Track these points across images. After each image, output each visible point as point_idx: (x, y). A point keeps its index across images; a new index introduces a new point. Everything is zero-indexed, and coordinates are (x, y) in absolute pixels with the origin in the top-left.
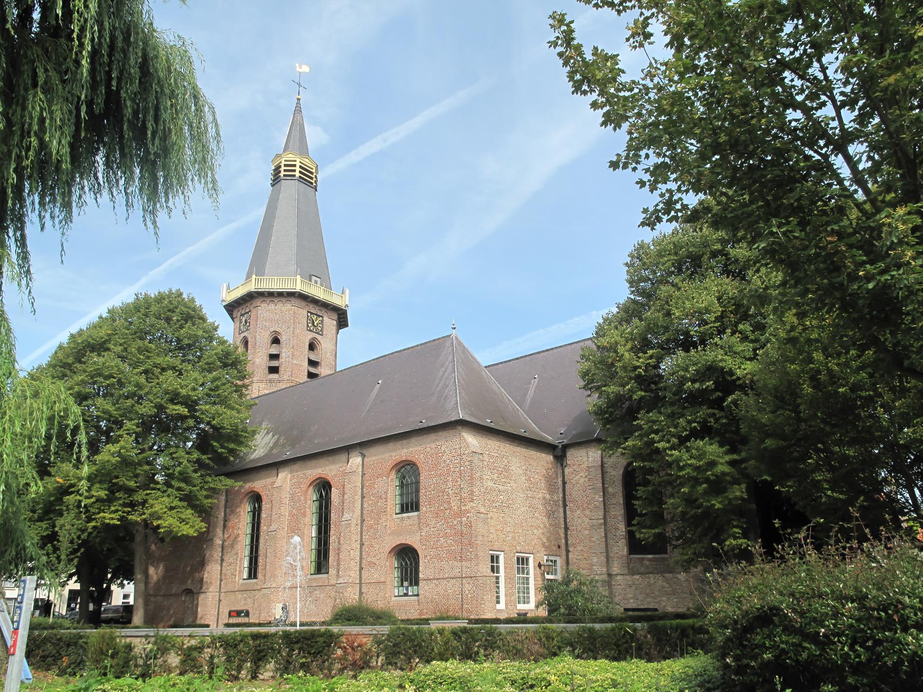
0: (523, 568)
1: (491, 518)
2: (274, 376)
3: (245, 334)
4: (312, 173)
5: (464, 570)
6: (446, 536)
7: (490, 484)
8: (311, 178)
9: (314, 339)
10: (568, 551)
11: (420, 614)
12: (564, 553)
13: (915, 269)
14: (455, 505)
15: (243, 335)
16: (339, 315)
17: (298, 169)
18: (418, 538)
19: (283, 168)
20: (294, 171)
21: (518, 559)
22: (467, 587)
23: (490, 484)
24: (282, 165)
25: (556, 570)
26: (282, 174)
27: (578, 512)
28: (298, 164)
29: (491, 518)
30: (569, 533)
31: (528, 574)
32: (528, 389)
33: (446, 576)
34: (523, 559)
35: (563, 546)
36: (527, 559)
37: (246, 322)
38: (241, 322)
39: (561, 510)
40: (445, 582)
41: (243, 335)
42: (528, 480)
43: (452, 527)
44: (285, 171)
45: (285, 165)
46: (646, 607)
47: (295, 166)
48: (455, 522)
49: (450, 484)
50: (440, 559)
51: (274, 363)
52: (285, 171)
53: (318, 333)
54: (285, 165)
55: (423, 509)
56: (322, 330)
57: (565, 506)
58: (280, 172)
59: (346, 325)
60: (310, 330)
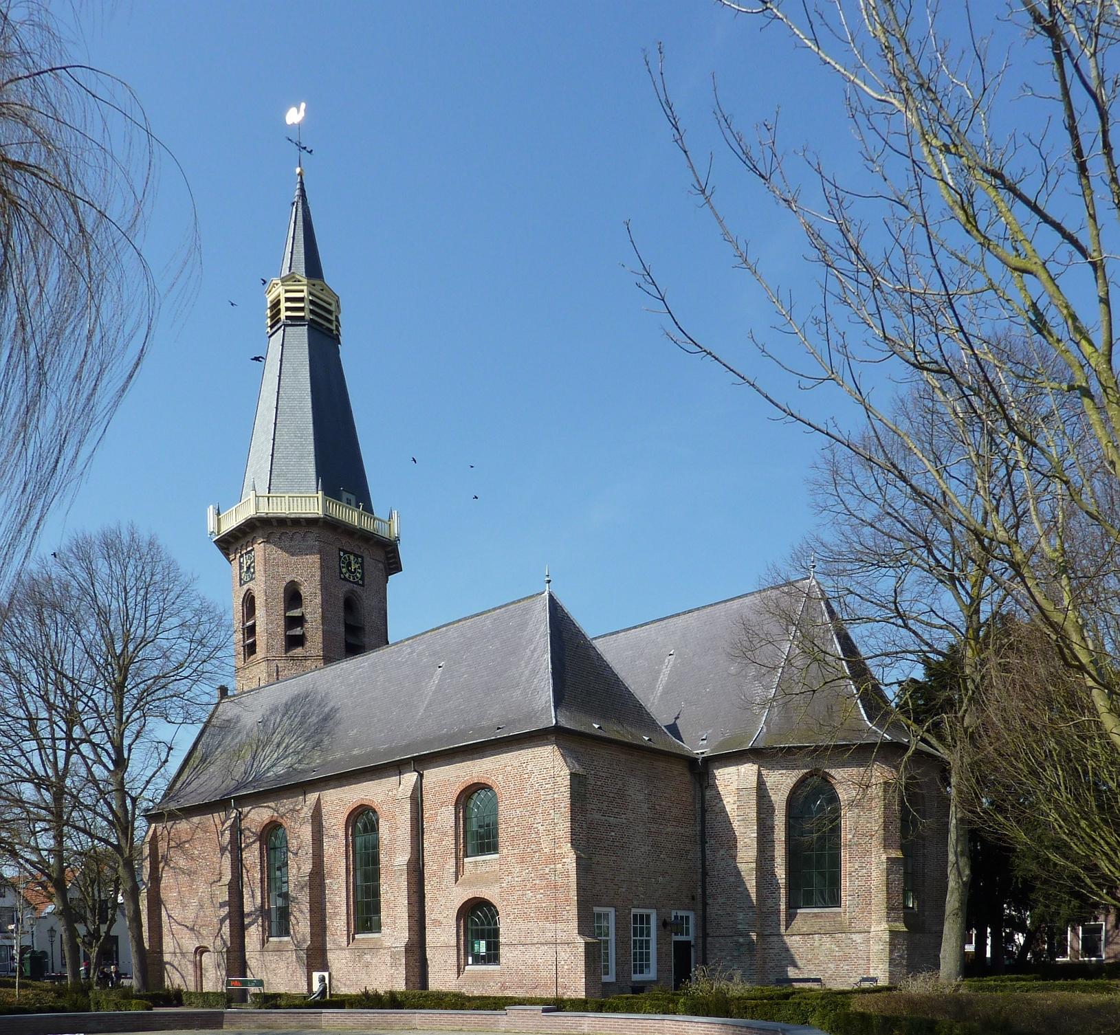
0: (642, 929)
1: (598, 863)
2: (298, 651)
3: (250, 585)
4: (330, 312)
5: (560, 934)
6: (534, 888)
7: (597, 816)
8: (330, 321)
9: (352, 592)
10: (705, 904)
11: (503, 987)
12: (700, 906)
13: (3, 674)
14: (546, 848)
15: (245, 587)
16: (387, 553)
18: (498, 890)
19: (283, 305)
21: (635, 916)
22: (563, 955)
23: (597, 816)
24: (283, 300)
25: (688, 929)
26: (284, 314)
27: (722, 852)
29: (598, 863)
30: (708, 879)
31: (648, 935)
32: (659, 672)
33: (536, 940)
34: (641, 916)
35: (699, 898)
36: (648, 917)
37: (248, 568)
38: (241, 567)
39: (698, 848)
40: (534, 948)
41: (245, 587)
42: (652, 808)
43: (542, 877)
44: (288, 309)
45: (287, 300)
46: (806, 976)
48: (547, 871)
49: (539, 818)
50: (527, 918)
51: (297, 631)
52: (288, 309)
53: (357, 583)
54: (287, 300)
55: (504, 851)
56: (362, 579)
57: (703, 842)
58: (279, 312)
59: (397, 568)
60: (345, 579)
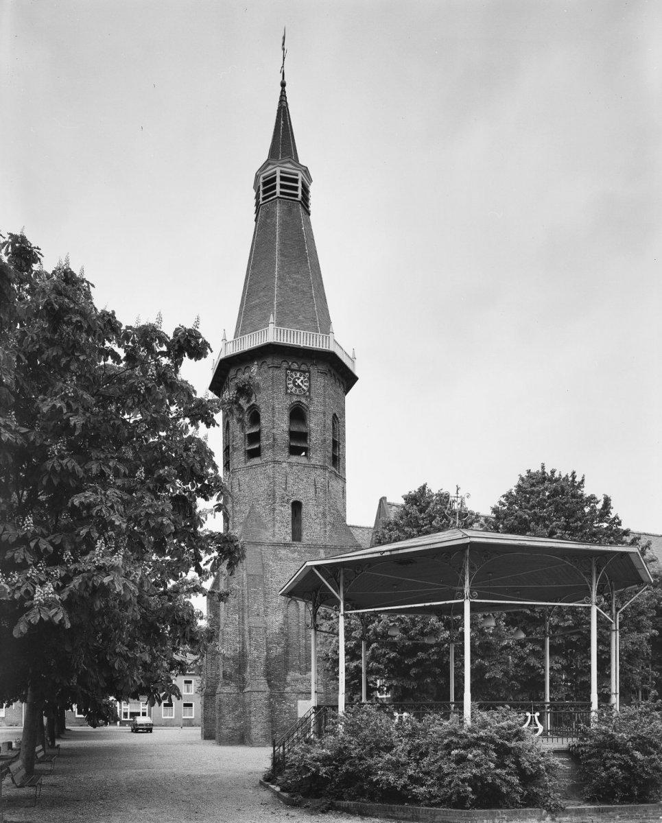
2: (256, 461)
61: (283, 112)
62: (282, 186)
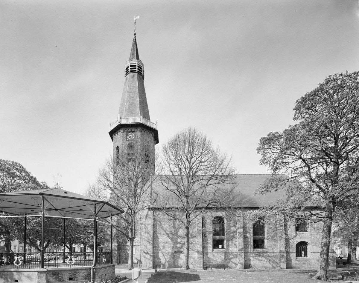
17: (137, 67)
20: (135, 68)
26: (129, 71)
28: (137, 64)
44: (131, 69)
45: (131, 66)
47: (135, 66)
61: (135, 43)
62: (138, 69)
